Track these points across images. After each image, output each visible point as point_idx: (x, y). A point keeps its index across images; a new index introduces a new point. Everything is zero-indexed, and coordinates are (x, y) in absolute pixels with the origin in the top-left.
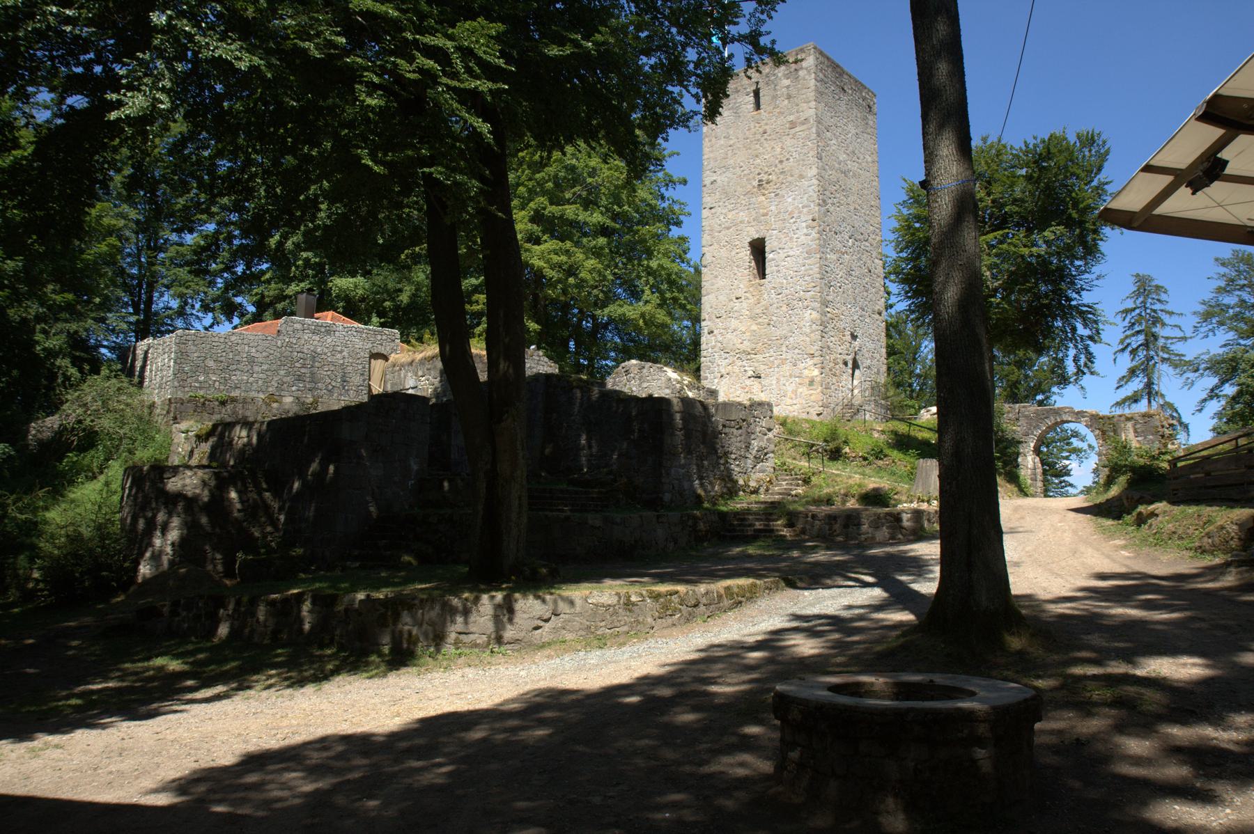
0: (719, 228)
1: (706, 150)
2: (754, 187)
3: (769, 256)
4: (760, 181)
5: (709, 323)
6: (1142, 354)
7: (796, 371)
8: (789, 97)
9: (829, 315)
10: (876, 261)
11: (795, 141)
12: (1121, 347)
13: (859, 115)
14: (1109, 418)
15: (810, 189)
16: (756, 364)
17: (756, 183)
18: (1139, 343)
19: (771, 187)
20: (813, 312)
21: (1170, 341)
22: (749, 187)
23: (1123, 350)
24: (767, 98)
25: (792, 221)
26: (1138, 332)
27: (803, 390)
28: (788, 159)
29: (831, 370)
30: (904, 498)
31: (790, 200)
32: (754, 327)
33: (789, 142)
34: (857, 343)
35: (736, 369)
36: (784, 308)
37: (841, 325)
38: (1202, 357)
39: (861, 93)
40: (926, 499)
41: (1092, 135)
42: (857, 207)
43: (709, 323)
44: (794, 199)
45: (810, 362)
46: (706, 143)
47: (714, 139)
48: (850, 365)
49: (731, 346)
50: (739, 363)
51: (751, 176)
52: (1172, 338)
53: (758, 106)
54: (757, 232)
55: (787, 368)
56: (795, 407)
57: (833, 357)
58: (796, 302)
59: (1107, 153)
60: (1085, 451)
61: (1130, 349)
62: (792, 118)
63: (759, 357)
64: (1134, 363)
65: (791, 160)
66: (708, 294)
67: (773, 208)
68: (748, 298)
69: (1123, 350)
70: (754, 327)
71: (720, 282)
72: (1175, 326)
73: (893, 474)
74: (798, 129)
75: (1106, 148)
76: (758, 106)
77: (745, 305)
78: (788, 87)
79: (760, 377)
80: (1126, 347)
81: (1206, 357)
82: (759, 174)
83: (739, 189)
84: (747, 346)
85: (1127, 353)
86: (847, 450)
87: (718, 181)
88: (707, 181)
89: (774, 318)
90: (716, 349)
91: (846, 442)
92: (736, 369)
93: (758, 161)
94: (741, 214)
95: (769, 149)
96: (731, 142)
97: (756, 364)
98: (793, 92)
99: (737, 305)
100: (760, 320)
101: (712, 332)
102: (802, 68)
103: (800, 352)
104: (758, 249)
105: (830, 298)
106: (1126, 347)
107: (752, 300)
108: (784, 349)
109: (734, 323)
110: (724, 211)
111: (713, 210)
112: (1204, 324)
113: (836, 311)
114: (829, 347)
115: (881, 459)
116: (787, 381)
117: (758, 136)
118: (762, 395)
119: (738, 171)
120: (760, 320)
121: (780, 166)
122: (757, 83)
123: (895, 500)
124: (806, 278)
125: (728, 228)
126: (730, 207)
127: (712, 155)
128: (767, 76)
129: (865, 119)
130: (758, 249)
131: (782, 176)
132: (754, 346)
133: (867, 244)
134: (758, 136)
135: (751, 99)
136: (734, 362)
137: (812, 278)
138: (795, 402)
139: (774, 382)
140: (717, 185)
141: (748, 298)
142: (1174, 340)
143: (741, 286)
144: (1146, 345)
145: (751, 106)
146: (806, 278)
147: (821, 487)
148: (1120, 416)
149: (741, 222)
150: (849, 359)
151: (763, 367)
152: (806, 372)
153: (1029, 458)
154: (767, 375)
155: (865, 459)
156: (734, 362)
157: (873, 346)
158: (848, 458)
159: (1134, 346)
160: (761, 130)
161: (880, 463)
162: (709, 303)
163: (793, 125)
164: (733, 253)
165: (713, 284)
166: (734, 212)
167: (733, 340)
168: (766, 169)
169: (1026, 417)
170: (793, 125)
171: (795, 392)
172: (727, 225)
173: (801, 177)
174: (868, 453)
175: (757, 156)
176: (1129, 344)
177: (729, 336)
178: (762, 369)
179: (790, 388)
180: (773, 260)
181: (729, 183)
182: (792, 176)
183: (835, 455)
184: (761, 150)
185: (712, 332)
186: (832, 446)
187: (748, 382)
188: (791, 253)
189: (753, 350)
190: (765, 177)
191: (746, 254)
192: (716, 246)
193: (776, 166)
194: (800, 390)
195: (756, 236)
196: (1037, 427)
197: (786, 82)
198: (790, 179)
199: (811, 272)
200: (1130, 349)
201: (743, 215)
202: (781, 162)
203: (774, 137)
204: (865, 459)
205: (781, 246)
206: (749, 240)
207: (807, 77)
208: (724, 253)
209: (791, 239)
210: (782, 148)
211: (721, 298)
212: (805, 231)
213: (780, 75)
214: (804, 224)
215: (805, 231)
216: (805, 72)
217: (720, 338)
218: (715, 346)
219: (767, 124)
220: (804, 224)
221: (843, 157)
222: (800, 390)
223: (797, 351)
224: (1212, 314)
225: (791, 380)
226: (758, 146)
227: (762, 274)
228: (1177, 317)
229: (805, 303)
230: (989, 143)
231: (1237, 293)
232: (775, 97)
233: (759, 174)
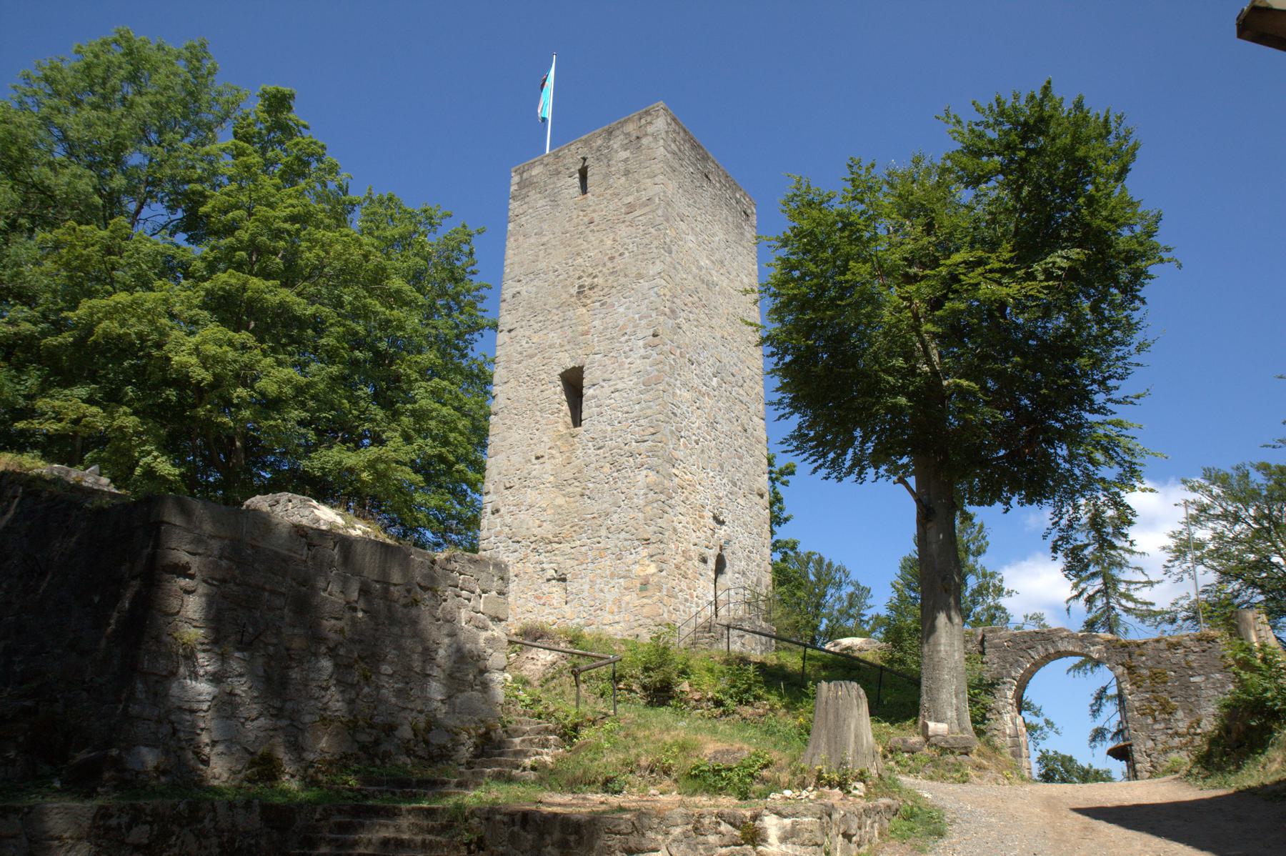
0: (517, 357)
1: (509, 252)
2: (572, 296)
3: (588, 392)
4: (580, 287)
5: (494, 497)
6: (1099, 603)
7: (621, 568)
8: (627, 173)
9: (676, 480)
10: (756, 419)
11: (633, 230)
12: (1075, 593)
13: (730, 219)
14: (1138, 646)
15: (652, 292)
16: (560, 559)
17: (574, 291)
18: (1096, 588)
19: (595, 295)
20: (651, 473)
21: (1133, 587)
22: (565, 296)
23: (1077, 597)
24: (596, 177)
25: (623, 339)
26: (1094, 575)
27: (631, 598)
28: (621, 255)
29: (678, 567)
30: (785, 777)
31: (621, 310)
32: (560, 501)
33: (623, 231)
34: (722, 532)
35: (529, 567)
36: (607, 469)
37: (697, 499)
38: (1181, 602)
39: (734, 192)
40: (836, 777)
41: (1106, 121)
42: (726, 335)
43: (494, 497)
44: (628, 308)
45: (644, 552)
46: (511, 243)
47: (521, 238)
48: (712, 563)
49: (524, 532)
50: (534, 558)
51: (568, 283)
52: (1136, 583)
53: (584, 189)
54: (572, 358)
55: (607, 562)
56: (618, 627)
57: (682, 547)
58: (624, 459)
59: (1135, 148)
60: (1041, 729)
61: (1085, 595)
62: (630, 199)
63: (565, 547)
64: (1090, 616)
65: (627, 254)
66: (496, 454)
67: (597, 323)
68: (553, 457)
69: (1077, 597)
70: (560, 501)
71: (514, 436)
72: (1137, 568)
73: (770, 732)
74: (637, 213)
75: (1131, 143)
76: (584, 189)
77: (548, 466)
78: (626, 160)
79: (564, 580)
80: (1080, 594)
81: (1185, 603)
82: (580, 278)
83: (551, 301)
84: (548, 530)
85: (1082, 601)
86: (685, 686)
87: (524, 293)
88: (507, 294)
89: (591, 485)
90: (502, 537)
91: (684, 673)
92: (529, 567)
93: (580, 260)
94: (552, 334)
95: (596, 243)
96: (545, 239)
97: (560, 559)
98: (633, 166)
99: (537, 468)
100: (570, 489)
101: (498, 511)
102: (646, 135)
103: (628, 536)
104: (573, 384)
105: (679, 454)
106: (1080, 594)
107: (559, 459)
108: (603, 532)
109: (531, 496)
110: (527, 333)
111: (513, 333)
112: (1177, 563)
113: (689, 477)
114: (675, 530)
115: (748, 703)
116: (607, 583)
117: (582, 228)
118: (567, 609)
119: (551, 275)
120: (570, 489)
121: (609, 265)
122: (585, 159)
123: (763, 780)
124: (642, 422)
125: (531, 357)
126: (536, 326)
127: (517, 259)
128: (598, 150)
129: (739, 226)
130: (573, 384)
131: (612, 278)
132: (558, 530)
133: (741, 391)
134: (582, 228)
135: (576, 180)
136: (526, 556)
137: (651, 422)
138: (617, 618)
139: (586, 587)
140: (519, 298)
141: (553, 457)
142: (1139, 586)
143: (545, 439)
144: (1104, 592)
145: (576, 190)
146: (642, 422)
147: (598, 749)
148: (1158, 641)
149: (550, 347)
150: (712, 555)
151: (570, 563)
152: (637, 569)
153: (1007, 718)
154: (575, 576)
155: (718, 703)
156: (526, 556)
157: (749, 542)
158: (686, 703)
159: (1091, 593)
160: (586, 220)
161: (747, 711)
162: (498, 463)
163: (631, 208)
164: (536, 392)
165: (504, 440)
166: (541, 334)
167: (529, 523)
168: (590, 270)
169: (997, 647)
170: (631, 208)
171: (618, 602)
172: (530, 351)
173: (640, 276)
174: (725, 693)
175: (578, 254)
176: (1084, 590)
177: (522, 516)
178: (568, 565)
179: (610, 596)
180: (594, 397)
181: (537, 293)
182: (626, 276)
183: (661, 694)
184: (585, 245)
185: (498, 511)
186: (656, 677)
187: (546, 588)
188: (620, 386)
189: (555, 536)
190: (587, 281)
191: (557, 393)
192: (513, 383)
193: (604, 265)
194: (627, 598)
195: (570, 365)
196: (1016, 664)
197: (624, 154)
198: (622, 280)
199: (649, 412)
200: (1085, 595)
201: (554, 337)
202: (612, 259)
203: (603, 227)
204: (718, 703)
205: (606, 376)
206: (560, 370)
207: (652, 145)
208: (523, 392)
209: (621, 365)
210: (615, 240)
211: (513, 458)
212: (642, 352)
213: (615, 146)
214: (641, 343)
215: (642, 352)
216: (650, 139)
217: (508, 520)
218: (500, 532)
219: (594, 211)
220: (641, 343)
221: (704, 262)
222: (627, 598)
223: (623, 535)
224: (1184, 548)
225: (613, 583)
226: (580, 241)
227: (577, 420)
228: (1138, 556)
229: (639, 460)
230: (924, 165)
231: (1211, 525)
232: (607, 176)
233: (580, 278)
